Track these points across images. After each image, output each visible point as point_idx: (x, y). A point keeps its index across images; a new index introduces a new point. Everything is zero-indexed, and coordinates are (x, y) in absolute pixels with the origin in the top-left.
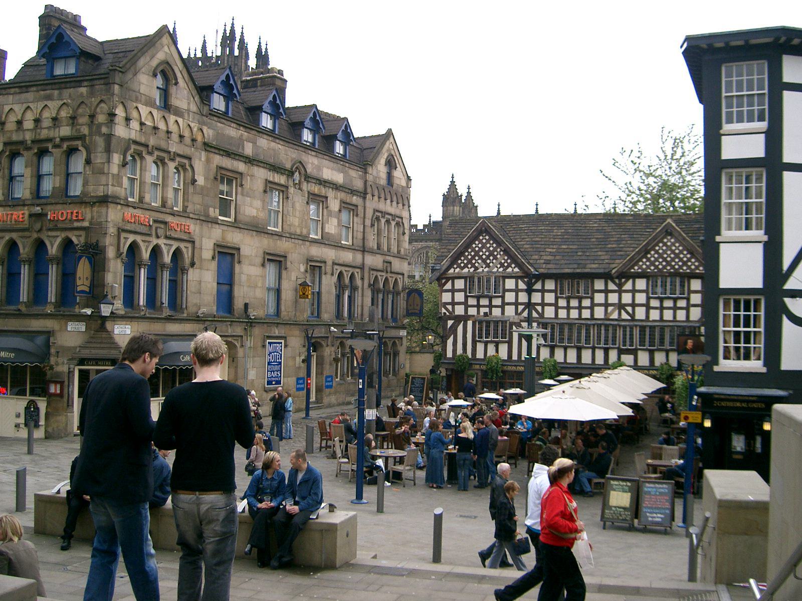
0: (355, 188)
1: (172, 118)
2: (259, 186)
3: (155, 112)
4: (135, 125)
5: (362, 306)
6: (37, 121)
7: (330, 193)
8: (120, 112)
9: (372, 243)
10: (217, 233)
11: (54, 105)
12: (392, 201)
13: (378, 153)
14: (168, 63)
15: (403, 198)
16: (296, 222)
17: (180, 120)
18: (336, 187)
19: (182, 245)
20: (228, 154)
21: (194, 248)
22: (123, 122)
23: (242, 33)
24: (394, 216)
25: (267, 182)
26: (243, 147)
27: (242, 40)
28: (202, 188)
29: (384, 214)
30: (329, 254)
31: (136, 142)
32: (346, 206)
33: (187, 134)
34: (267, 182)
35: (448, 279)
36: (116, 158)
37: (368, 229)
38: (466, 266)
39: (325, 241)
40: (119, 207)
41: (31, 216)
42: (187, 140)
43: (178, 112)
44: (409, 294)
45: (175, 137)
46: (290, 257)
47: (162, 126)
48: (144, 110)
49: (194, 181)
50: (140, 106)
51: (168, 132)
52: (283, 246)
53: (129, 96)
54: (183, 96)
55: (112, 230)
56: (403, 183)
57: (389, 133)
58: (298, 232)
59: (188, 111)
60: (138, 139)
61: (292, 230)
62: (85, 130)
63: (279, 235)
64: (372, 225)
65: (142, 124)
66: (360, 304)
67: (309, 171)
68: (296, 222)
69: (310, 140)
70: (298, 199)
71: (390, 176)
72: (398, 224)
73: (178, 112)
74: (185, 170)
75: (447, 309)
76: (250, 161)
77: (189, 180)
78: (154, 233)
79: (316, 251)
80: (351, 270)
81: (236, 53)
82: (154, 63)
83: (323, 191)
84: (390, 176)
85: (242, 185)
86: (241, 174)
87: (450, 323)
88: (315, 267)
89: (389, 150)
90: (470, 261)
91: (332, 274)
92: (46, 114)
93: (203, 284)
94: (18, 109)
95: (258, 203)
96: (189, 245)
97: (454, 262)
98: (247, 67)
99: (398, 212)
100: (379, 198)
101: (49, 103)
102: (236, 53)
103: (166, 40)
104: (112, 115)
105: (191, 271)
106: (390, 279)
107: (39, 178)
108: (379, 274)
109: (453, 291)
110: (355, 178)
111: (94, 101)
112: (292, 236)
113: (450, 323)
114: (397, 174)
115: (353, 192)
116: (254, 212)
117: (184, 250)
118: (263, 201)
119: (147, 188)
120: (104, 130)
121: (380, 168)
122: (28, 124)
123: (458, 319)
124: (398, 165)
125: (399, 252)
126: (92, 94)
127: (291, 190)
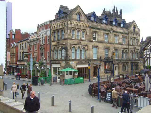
0: (126, 33)
1: (81, 22)
2: (102, 34)
3: (77, 22)
4: (73, 24)
5: (129, 56)
6: (57, 26)
7: (120, 34)
8: (69, 22)
9: (131, 43)
10: (93, 44)
11: (59, 23)
12: (135, 35)
13: (131, 25)
14: (79, 12)
15: (138, 34)
16: (112, 40)
17: (83, 23)
18: (121, 33)
19: (85, 46)
20: (94, 28)
21: (87, 47)
22: (70, 24)
23: (116, 8)
24: (136, 38)
25: (104, 33)
26: (98, 27)
27: (116, 10)
28: (89, 35)
29: (133, 38)
30: (120, 46)
31: (73, 28)
32: (124, 37)
33: (85, 25)
34: (104, 33)
35: (145, 50)
36: (69, 31)
37: (129, 41)
38: (149, 47)
39: (119, 44)
40: (70, 40)
41: (57, 43)
42: (85, 26)
43: (82, 21)
44: (140, 53)
45: (82, 26)
46: (110, 47)
47: (79, 24)
48: (74, 21)
49: (87, 34)
50: (73, 21)
51: (80, 25)
52: (108, 45)
53: (71, 19)
54: (83, 18)
55: (69, 44)
56: (138, 31)
57: (134, 21)
58: (112, 42)
59: (85, 21)
60: (74, 27)
61: (111, 42)
62: (64, 26)
63: (108, 43)
64: (130, 40)
65: (74, 24)
66: (128, 56)
67: (114, 30)
68: (112, 40)
69: (123, 26)
70: (112, 36)
71: (134, 30)
72: (137, 39)
73: (82, 21)
74: (85, 32)
75: (145, 56)
76: (99, 29)
77: (86, 34)
78: (78, 44)
79: (116, 46)
80: (126, 49)
81: (116, 12)
82: (76, 12)
83: (118, 34)
84: (134, 30)
85: (98, 34)
86: (98, 32)
87: (146, 59)
88: (116, 49)
89: (134, 24)
90: (149, 46)
91: (121, 50)
92: (58, 25)
93: (90, 53)
94: (54, 24)
95: (102, 37)
96: (86, 46)
97: (146, 46)
98: (118, 14)
99: (137, 37)
100: (132, 34)
101: (58, 22)
102: (116, 12)
103: (79, 8)
104: (68, 23)
105: (87, 51)
106: (136, 51)
107: (58, 36)
108: (132, 50)
109: (146, 52)
110: (126, 31)
111: (65, 21)
112: (111, 43)
113: (146, 59)
114: (136, 29)
115: (125, 34)
116: (101, 39)
117: (85, 47)
118: (103, 37)
119: (76, 36)
120: (66, 26)
121: (132, 29)
122: (56, 27)
123: (148, 58)
124: (136, 27)
125: (138, 45)
126: (64, 20)
127: (110, 34)
